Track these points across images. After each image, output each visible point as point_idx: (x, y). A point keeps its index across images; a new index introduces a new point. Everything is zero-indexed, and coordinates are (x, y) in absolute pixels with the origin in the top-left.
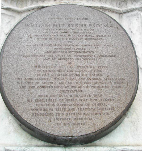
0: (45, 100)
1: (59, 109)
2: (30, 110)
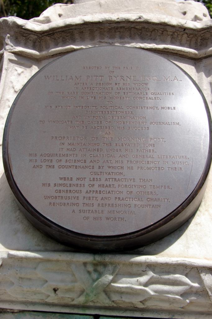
0: (68, 185)
1: (88, 198)
2: (46, 197)
